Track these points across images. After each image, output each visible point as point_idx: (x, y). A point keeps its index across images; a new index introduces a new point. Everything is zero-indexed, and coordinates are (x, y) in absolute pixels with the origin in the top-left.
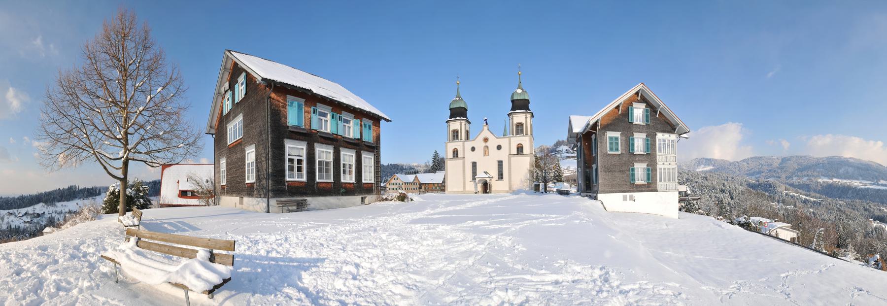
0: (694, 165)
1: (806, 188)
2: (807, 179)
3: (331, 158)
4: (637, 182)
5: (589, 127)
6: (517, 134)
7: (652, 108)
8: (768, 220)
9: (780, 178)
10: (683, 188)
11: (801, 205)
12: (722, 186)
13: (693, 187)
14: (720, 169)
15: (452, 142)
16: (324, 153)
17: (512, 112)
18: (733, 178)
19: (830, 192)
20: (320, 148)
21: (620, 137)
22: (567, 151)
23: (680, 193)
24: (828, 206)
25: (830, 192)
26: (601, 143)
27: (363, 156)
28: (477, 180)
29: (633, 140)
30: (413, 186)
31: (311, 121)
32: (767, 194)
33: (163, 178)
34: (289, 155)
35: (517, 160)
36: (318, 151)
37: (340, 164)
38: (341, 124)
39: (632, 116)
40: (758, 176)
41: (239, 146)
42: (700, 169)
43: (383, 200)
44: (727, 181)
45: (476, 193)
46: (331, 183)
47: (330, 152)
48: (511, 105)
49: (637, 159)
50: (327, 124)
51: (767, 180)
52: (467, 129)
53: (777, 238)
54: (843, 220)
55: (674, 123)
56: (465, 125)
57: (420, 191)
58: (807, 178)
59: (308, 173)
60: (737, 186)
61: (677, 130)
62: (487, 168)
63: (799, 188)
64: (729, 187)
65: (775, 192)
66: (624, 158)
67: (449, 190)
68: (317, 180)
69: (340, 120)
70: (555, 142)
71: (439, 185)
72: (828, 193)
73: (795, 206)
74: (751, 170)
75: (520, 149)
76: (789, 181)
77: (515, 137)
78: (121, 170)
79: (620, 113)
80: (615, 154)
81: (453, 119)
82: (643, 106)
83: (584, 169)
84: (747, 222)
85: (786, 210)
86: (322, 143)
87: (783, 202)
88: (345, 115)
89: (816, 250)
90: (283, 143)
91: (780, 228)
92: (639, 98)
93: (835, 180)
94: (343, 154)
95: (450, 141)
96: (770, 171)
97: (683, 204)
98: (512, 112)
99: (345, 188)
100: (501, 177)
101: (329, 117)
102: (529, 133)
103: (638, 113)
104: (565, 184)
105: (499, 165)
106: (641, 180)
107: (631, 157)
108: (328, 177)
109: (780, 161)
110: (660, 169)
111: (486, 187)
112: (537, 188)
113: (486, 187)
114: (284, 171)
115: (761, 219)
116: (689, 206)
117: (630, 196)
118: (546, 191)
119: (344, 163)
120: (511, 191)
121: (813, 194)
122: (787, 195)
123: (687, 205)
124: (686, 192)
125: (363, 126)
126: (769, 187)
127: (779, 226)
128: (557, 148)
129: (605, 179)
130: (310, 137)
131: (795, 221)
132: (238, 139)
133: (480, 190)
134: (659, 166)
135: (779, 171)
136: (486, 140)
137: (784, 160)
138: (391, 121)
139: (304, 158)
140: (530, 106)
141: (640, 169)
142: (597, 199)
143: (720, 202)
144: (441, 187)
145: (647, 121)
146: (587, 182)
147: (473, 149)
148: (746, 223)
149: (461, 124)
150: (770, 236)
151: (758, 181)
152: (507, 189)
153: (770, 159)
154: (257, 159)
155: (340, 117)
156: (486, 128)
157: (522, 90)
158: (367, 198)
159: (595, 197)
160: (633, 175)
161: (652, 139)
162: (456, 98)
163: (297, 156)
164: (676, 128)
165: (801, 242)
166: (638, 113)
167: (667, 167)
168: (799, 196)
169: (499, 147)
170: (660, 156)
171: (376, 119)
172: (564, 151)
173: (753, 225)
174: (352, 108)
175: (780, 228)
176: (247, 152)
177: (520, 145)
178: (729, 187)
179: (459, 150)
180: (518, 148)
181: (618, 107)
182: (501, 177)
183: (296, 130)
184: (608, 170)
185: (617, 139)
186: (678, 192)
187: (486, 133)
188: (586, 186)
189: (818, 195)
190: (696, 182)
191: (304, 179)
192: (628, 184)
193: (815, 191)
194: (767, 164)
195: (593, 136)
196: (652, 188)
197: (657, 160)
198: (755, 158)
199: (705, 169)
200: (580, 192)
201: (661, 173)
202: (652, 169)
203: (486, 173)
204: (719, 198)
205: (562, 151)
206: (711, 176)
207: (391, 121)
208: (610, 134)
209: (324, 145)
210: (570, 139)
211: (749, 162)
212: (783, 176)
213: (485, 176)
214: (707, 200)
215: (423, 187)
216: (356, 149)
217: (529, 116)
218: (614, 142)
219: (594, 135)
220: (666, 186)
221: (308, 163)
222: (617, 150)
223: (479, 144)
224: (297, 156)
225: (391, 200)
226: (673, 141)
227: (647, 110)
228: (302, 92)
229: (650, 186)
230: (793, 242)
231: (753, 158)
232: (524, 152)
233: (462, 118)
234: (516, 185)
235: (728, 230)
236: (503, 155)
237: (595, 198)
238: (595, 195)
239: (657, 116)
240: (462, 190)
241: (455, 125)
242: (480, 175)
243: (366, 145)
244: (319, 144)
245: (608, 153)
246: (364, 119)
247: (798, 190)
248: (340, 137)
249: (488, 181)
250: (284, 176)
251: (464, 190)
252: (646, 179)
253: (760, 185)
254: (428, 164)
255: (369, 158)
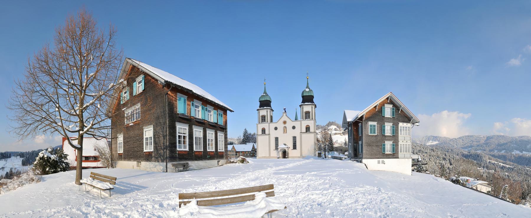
0: (425, 140)
1: (504, 158)
2: (505, 152)
3: (201, 135)
4: (386, 153)
5: (358, 118)
6: (306, 119)
7: (396, 107)
8: (473, 179)
9: (485, 150)
10: (416, 157)
11: (499, 170)
12: (444, 155)
13: (423, 156)
14: (443, 143)
15: (261, 124)
16: (198, 132)
17: (302, 104)
18: (452, 150)
19: (520, 161)
20: (220, 133)
21: (376, 125)
22: (335, 130)
23: (413, 160)
24: (519, 171)
25: (520, 161)
26: (365, 128)
27: (207, 132)
28: (279, 149)
29: (384, 127)
30: (232, 153)
31: (190, 111)
32: (475, 161)
33: (64, 144)
34: (179, 133)
35: (306, 136)
36: (178, 128)
37: (206, 139)
38: (207, 113)
39: (384, 112)
40: (470, 149)
41: (139, 126)
42: (430, 143)
43: (231, 162)
44: (448, 152)
45: (278, 158)
46: (202, 152)
47: (186, 129)
48: (301, 99)
49: (387, 138)
50: (199, 113)
51: (476, 152)
52: (271, 115)
53: (477, 190)
54: (528, 181)
55: (410, 117)
56: (270, 112)
57: (236, 157)
58: (504, 151)
59: (189, 145)
60: (455, 156)
61: (411, 121)
62: (286, 142)
63: (498, 158)
64: (449, 156)
65: (482, 161)
66: (379, 138)
67: (259, 156)
68: (195, 150)
69: (206, 110)
70: (328, 122)
71: (249, 152)
72: (519, 162)
73: (495, 171)
74: (465, 145)
75: (308, 129)
76: (492, 153)
77: (304, 121)
78: (77, 140)
79: (377, 110)
80: (373, 136)
81: (262, 108)
82: (391, 106)
83: (353, 144)
84: (457, 179)
85: (489, 173)
86: (197, 125)
87: (487, 167)
88: (209, 108)
89: (502, 199)
90: (175, 125)
91: (480, 184)
92: (389, 101)
93: (524, 152)
94: (195, 130)
95: (259, 123)
96: (478, 146)
97: (416, 168)
98: (302, 104)
99: (210, 155)
100: (295, 147)
101: (200, 108)
102: (314, 118)
103: (388, 111)
104: (335, 152)
105: (293, 139)
106: (389, 151)
107: (383, 137)
108: (185, 147)
109: (486, 138)
110: (401, 145)
111: (285, 154)
112: (320, 155)
113: (285, 154)
114: (176, 143)
115: (468, 178)
116: (419, 169)
117: (382, 161)
118: (325, 157)
119: (209, 138)
120: (301, 157)
121: (508, 162)
122: (490, 163)
123: (418, 167)
124: (417, 159)
125: (218, 115)
126: (477, 157)
127: (480, 183)
128: (328, 127)
129: (367, 150)
130: (190, 121)
131: (492, 181)
132: (135, 120)
133: (281, 156)
134: (400, 143)
135: (485, 146)
136: (285, 122)
137: (488, 138)
138: (234, 112)
139: (187, 135)
140: (314, 100)
141: (388, 145)
142: (362, 163)
143: (442, 167)
144: (253, 153)
145: (393, 115)
146: (355, 152)
147: (276, 129)
148: (456, 180)
149: (267, 112)
150: (472, 189)
151: (469, 153)
152: (299, 155)
153: (479, 137)
154: (154, 136)
155: (206, 108)
156: (285, 114)
157: (309, 89)
158: (220, 161)
159: (361, 161)
160: (384, 148)
161: (396, 127)
162: (264, 94)
163: (183, 134)
164: (411, 120)
165: (495, 194)
166: (388, 111)
167: (405, 143)
168: (498, 164)
169: (294, 128)
170: (401, 137)
171: (224, 110)
172: (334, 129)
173: (462, 182)
174: (213, 103)
175: (480, 184)
176: (145, 130)
177: (308, 126)
178: (449, 156)
179: (265, 128)
180: (306, 128)
181: (375, 107)
182: (295, 147)
183: (183, 117)
184: (369, 145)
185: (374, 126)
186: (411, 159)
187: (285, 118)
188: (355, 154)
189: (512, 163)
190: (426, 153)
191: (187, 149)
192: (381, 153)
193: (510, 160)
194: (476, 141)
195: (360, 124)
196: (396, 157)
197: (399, 139)
198: (468, 136)
199: (433, 143)
200: (350, 157)
201: (401, 147)
202: (396, 145)
203: (285, 145)
204: (441, 164)
205: (332, 129)
206: (436, 148)
207: (234, 112)
208: (370, 123)
209: (198, 127)
210: (344, 125)
211: (464, 139)
212: (488, 149)
213: (284, 146)
214: (432, 165)
215: (238, 153)
216: (215, 129)
217: (313, 107)
218: (373, 128)
219: (360, 123)
220: (410, 155)
221: (189, 138)
222: (374, 133)
223: (280, 126)
224: (183, 134)
225: (236, 163)
226: (409, 128)
227: (393, 108)
228: (210, 102)
229: (394, 155)
230: (488, 193)
231: (466, 136)
232: (311, 131)
233: (268, 107)
234: (305, 153)
235: (441, 182)
236: (296, 133)
237: (361, 162)
238: (361, 160)
239: (400, 112)
240: (268, 156)
241: (263, 112)
242: (281, 146)
243: (219, 127)
244: (220, 132)
245: (369, 134)
246: (219, 110)
247: (498, 159)
248: (206, 121)
249: (287, 150)
250: (176, 147)
251: (270, 157)
252: (392, 150)
253: (471, 155)
254: (240, 138)
255: (211, 133)
